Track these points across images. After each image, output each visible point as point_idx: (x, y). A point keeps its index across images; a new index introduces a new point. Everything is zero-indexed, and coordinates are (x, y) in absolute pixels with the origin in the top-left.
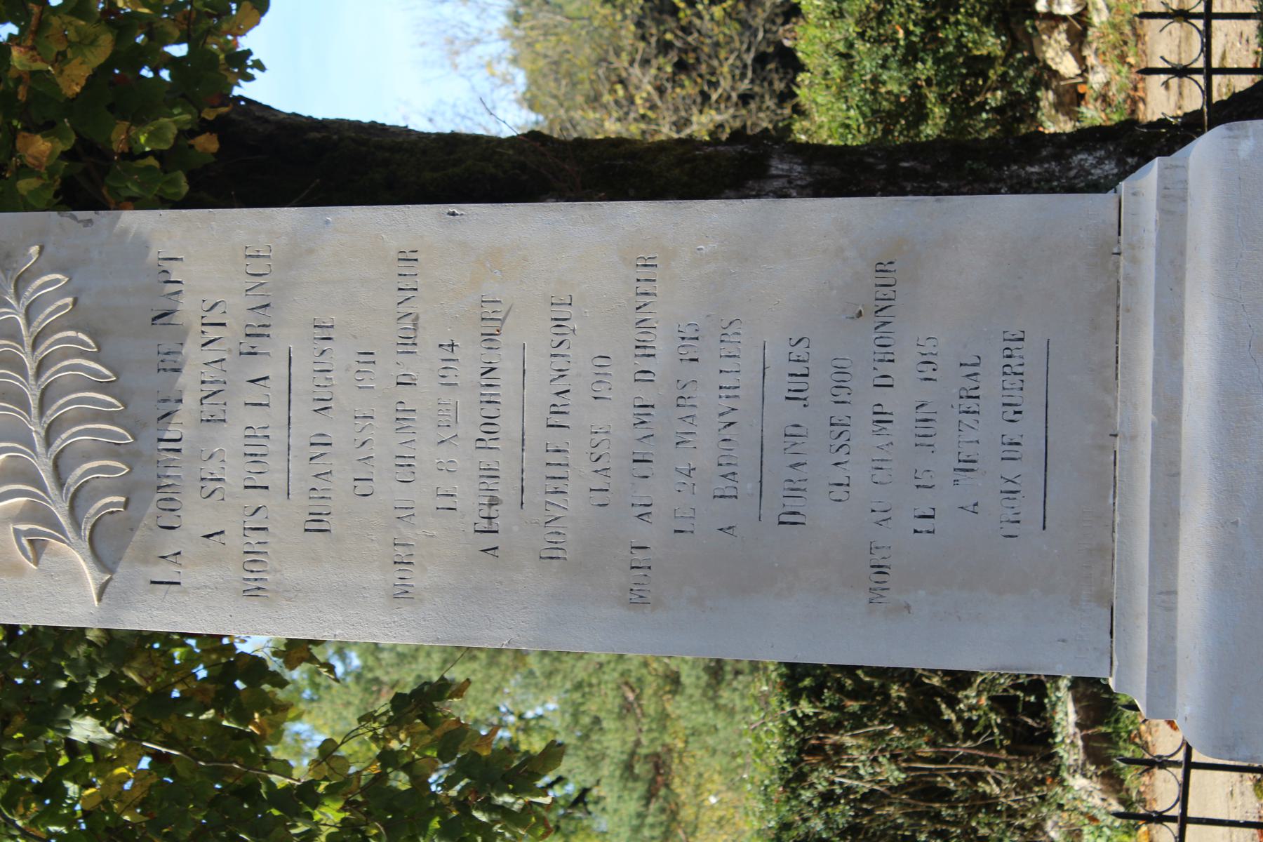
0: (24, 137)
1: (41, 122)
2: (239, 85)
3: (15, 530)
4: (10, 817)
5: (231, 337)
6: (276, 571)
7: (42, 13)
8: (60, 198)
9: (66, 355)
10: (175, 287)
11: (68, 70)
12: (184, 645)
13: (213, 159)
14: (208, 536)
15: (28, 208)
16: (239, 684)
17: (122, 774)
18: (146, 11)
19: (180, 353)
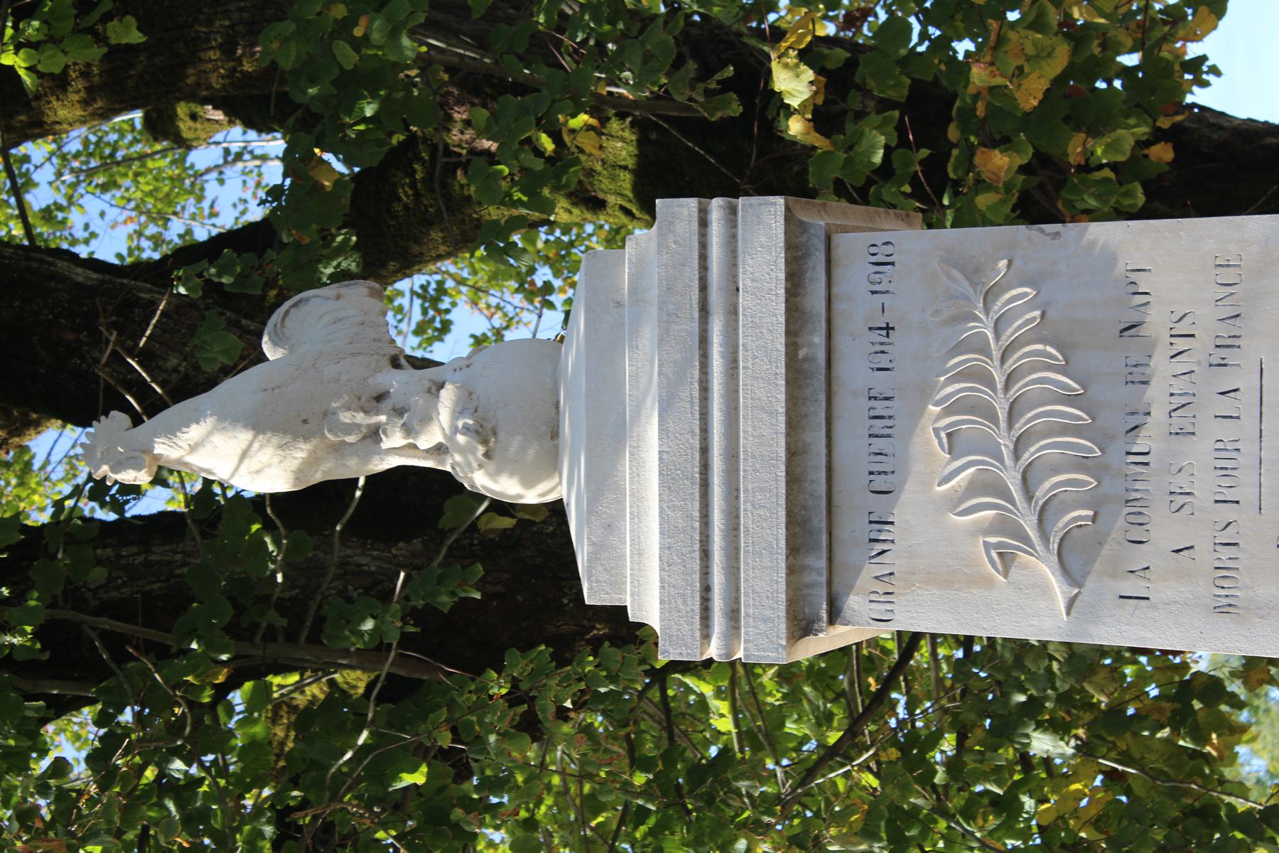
0: (983, 152)
1: (998, 137)
2: (1192, 93)
3: (985, 542)
4: (968, 828)
5: (1201, 348)
6: (1248, 588)
7: (1001, 28)
8: (1018, 212)
9: (1034, 368)
10: (1143, 299)
11: (1026, 84)
12: (1136, 662)
13: (1167, 168)
14: (1178, 551)
15: (986, 222)
16: (1197, 705)
17: (1077, 790)
18: (1102, 21)
19: (1148, 365)
